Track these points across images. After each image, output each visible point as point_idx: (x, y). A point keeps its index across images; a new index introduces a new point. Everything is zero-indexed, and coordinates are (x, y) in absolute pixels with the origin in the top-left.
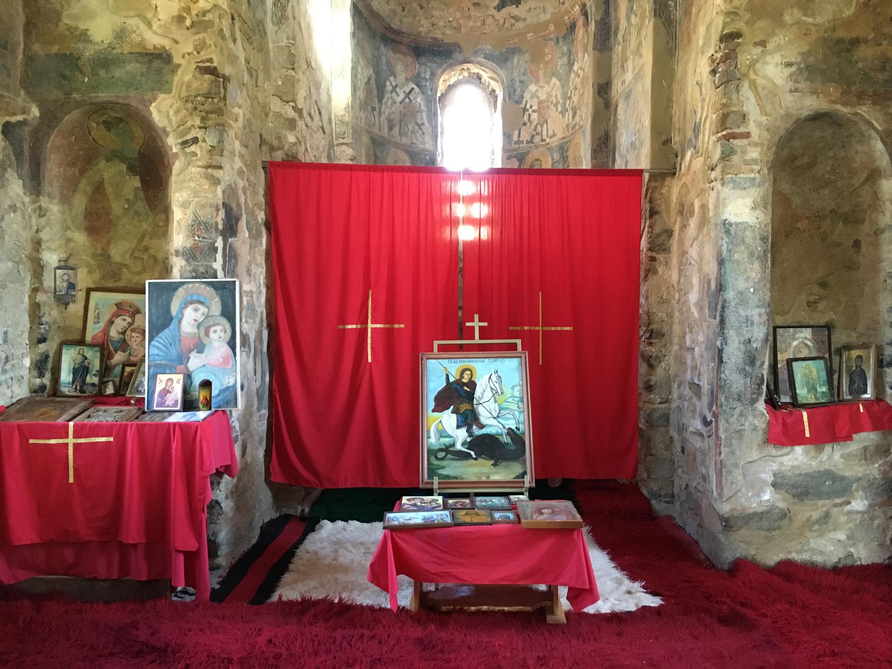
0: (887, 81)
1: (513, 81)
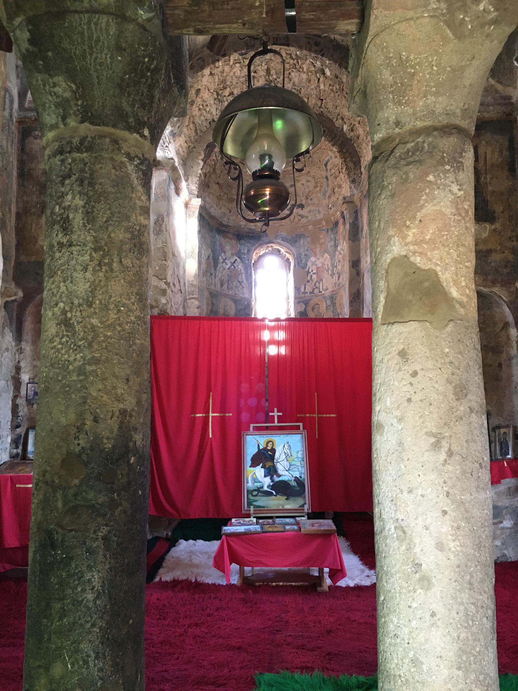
0: (508, 273)
1: (300, 254)
